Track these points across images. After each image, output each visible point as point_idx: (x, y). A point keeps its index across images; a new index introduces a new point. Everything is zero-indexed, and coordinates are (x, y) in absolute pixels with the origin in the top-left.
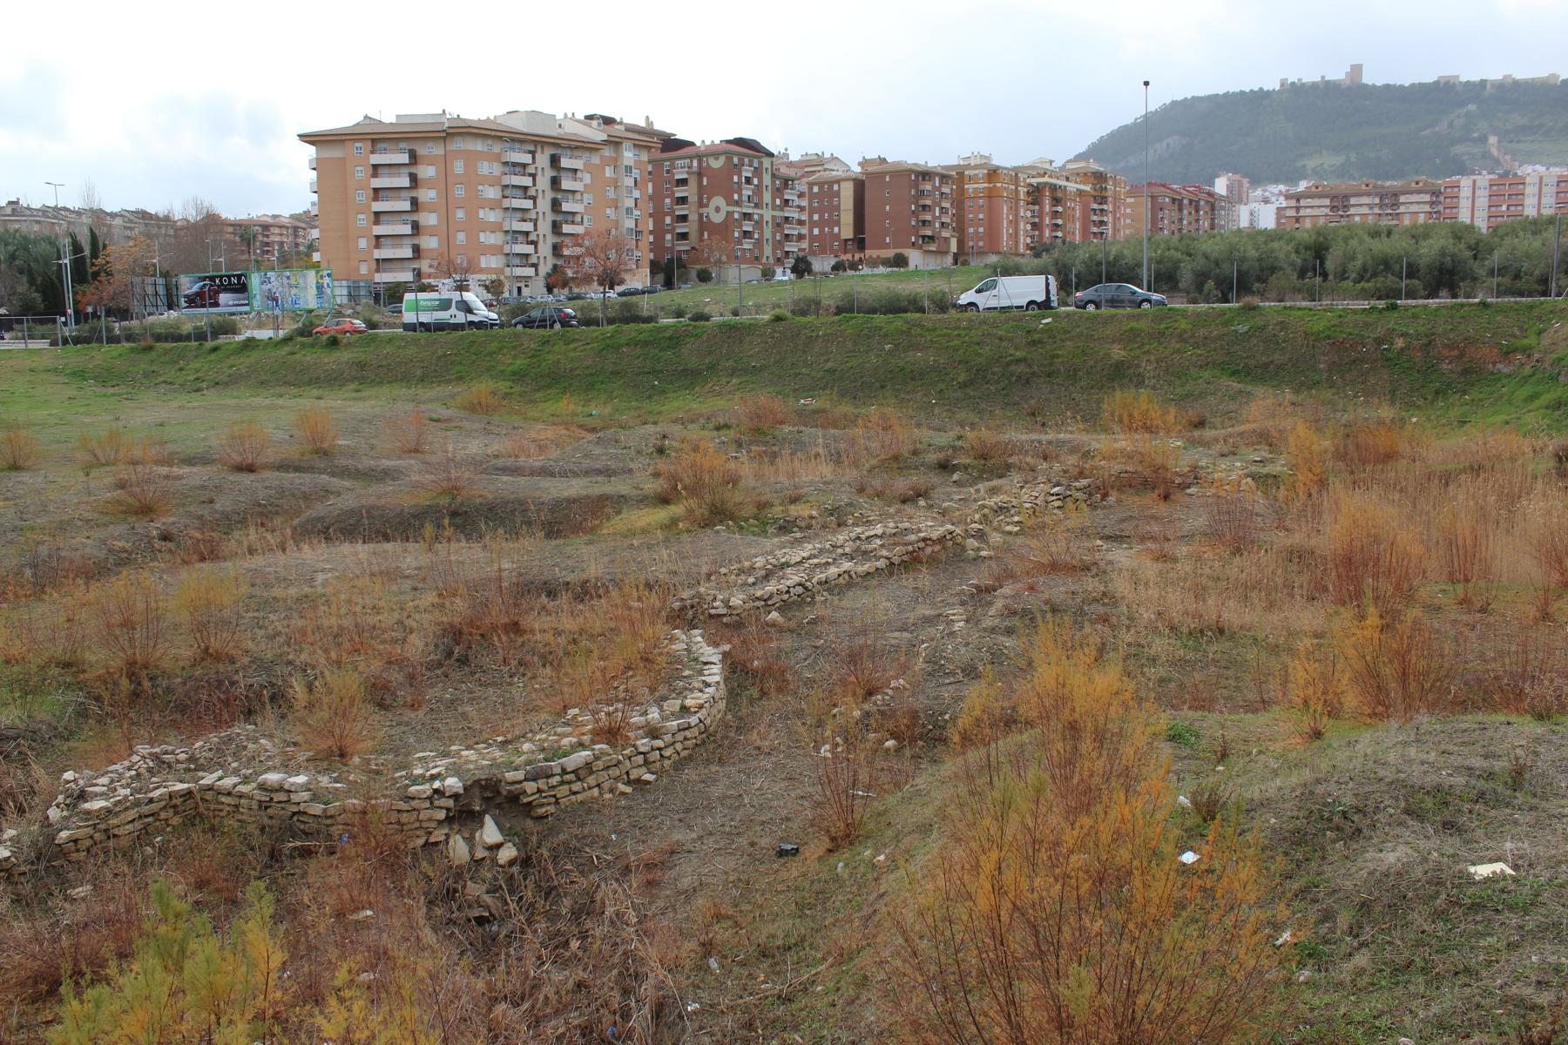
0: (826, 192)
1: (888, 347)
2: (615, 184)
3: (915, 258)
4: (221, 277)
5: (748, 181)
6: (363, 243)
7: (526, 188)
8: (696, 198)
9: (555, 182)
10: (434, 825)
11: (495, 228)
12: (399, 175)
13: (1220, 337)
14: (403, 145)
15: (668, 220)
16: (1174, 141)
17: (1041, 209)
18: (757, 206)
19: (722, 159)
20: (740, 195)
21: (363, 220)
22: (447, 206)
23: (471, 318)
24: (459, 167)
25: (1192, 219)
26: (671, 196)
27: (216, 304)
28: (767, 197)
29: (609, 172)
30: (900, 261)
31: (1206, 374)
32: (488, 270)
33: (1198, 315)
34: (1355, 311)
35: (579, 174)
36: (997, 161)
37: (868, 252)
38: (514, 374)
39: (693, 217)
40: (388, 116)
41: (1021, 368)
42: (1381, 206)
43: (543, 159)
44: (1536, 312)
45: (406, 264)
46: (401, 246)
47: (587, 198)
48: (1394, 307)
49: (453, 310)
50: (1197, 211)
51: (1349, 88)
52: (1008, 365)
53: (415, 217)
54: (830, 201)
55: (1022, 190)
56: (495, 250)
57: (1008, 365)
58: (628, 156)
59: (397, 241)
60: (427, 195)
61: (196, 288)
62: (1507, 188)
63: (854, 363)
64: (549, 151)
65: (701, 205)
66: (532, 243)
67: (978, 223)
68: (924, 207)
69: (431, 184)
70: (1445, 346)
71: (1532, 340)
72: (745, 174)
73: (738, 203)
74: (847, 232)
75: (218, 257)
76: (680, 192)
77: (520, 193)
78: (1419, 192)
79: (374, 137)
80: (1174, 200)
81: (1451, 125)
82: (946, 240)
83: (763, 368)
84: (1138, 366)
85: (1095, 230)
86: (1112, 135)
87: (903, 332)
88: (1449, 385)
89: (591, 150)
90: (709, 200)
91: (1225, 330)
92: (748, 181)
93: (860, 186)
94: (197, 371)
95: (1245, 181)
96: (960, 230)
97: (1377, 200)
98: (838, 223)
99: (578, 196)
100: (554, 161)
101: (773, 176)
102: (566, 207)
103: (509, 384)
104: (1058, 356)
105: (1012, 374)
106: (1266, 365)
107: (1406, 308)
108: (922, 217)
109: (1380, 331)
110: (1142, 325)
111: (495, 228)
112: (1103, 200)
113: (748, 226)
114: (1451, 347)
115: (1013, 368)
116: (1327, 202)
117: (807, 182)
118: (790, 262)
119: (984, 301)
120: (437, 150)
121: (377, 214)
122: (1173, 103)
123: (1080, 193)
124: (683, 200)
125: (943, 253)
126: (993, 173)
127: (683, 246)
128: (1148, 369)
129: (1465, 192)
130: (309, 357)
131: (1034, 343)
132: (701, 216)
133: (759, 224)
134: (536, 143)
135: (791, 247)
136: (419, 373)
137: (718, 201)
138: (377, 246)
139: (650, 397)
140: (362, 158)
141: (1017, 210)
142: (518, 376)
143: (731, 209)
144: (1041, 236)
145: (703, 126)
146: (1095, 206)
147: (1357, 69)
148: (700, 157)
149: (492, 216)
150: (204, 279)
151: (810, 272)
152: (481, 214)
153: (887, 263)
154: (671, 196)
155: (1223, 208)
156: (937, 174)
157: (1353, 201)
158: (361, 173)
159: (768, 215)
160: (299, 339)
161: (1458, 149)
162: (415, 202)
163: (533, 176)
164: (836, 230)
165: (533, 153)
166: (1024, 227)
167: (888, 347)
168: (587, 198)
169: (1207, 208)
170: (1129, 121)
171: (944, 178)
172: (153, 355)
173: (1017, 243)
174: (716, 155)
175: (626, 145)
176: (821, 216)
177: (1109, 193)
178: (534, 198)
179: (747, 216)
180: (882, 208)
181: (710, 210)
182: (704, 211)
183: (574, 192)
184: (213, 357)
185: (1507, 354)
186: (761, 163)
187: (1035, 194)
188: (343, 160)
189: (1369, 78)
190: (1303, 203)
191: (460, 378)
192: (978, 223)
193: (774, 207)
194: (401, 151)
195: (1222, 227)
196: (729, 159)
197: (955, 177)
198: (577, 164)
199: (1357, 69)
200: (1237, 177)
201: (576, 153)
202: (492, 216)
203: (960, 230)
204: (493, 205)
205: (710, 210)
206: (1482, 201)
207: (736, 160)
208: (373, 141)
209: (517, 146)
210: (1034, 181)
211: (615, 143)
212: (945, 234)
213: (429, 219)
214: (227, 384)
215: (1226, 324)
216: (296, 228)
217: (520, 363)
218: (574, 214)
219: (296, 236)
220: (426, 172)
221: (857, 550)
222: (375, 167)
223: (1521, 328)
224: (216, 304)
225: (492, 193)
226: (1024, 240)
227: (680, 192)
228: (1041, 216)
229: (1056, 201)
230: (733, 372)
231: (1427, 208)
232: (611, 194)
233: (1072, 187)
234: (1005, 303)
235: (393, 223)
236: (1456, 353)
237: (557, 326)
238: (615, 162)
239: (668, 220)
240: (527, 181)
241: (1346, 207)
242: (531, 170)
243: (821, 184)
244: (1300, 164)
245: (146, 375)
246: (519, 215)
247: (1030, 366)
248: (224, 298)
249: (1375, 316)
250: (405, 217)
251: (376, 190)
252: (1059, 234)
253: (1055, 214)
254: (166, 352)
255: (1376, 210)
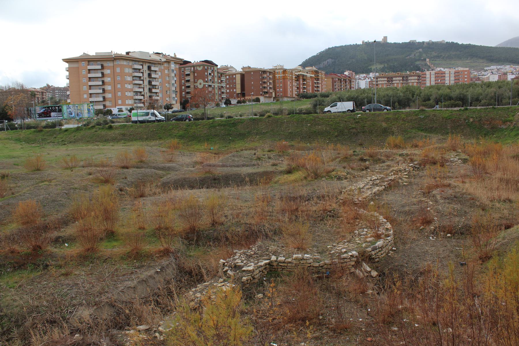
0: (232, 77)
1: (309, 125)
2: (169, 75)
3: (262, 99)
4: (52, 107)
5: (210, 74)
6: (85, 96)
7: (140, 77)
8: (193, 80)
9: (150, 75)
10: (351, 266)
11: (130, 90)
12: (97, 73)
13: (416, 119)
14: (99, 63)
15: (183, 87)
16: (330, 61)
17: (299, 83)
18: (213, 82)
19: (202, 67)
20: (208, 79)
21: (85, 88)
22: (114, 83)
23: (157, 118)
24: (118, 70)
25: (344, 85)
26: (184, 79)
27: (50, 116)
28: (216, 80)
29: (166, 72)
30: (258, 100)
31: (414, 131)
32: (129, 105)
33: (407, 113)
34: (455, 111)
35: (157, 72)
36: (286, 67)
37: (246, 98)
38: (180, 136)
39: (192, 86)
40: (92, 53)
41: (354, 130)
42: (403, 80)
43: (146, 67)
44: (510, 110)
45: (101, 103)
46: (98, 97)
47: (160, 80)
48: (467, 109)
49: (150, 116)
50: (346, 83)
51: (383, 44)
52: (350, 129)
53: (103, 87)
54: (233, 81)
55: (294, 77)
56: (131, 98)
57: (350, 129)
58: (173, 66)
59: (97, 95)
60: (107, 80)
61: (42, 111)
62: (440, 75)
63: (298, 130)
64: (147, 65)
65: (195, 82)
66: (143, 95)
67: (280, 87)
68: (264, 82)
69: (108, 75)
70: (485, 120)
71: (511, 118)
72: (209, 72)
73: (207, 82)
74: (238, 90)
75: (49, 102)
76: (187, 78)
77: (138, 79)
78: (414, 76)
79: (88, 60)
80: (339, 79)
81: (415, 55)
82: (271, 93)
83: (267, 132)
84: (392, 129)
85: (316, 89)
86: (310, 59)
87: (313, 120)
88: (488, 132)
89: (160, 64)
90: (197, 80)
91: (417, 117)
92: (210, 74)
93: (243, 76)
94: (62, 138)
95: (354, 73)
96: (275, 89)
97: (401, 78)
98: (235, 88)
99: (157, 80)
100: (149, 68)
101: (218, 72)
102: (153, 83)
103: (179, 140)
104: (365, 126)
105: (351, 132)
106: (431, 128)
107: (471, 109)
108: (264, 86)
109: (465, 117)
110: (390, 116)
111: (130, 90)
112: (318, 79)
113: (210, 89)
114: (487, 121)
115: (351, 130)
116: (386, 79)
117: (225, 74)
118: (224, 101)
119: (333, 110)
120: (110, 64)
121: (90, 86)
122: (329, 48)
123: (311, 77)
124: (188, 81)
125: (270, 97)
126: (285, 71)
127: (189, 96)
128: (395, 129)
129: (428, 76)
130: (103, 132)
131: (357, 122)
132: (195, 86)
133: (214, 88)
134: (143, 62)
135: (224, 96)
136: (145, 137)
137: (201, 81)
138: (91, 97)
139: (229, 143)
140: (85, 66)
141: (292, 83)
142: (181, 137)
143: (205, 83)
144: (300, 91)
145: (194, 56)
146: (316, 81)
147: (385, 38)
148: (194, 67)
149: (129, 87)
150: (45, 108)
151: (230, 104)
152: (126, 86)
153: (254, 101)
154: (184, 79)
155: (353, 82)
156: (268, 72)
157: (394, 79)
158: (84, 72)
159: (216, 85)
160: (97, 126)
161: (417, 63)
162: (103, 82)
163: (143, 73)
164: (235, 90)
165: (142, 65)
166: (295, 88)
167: (309, 125)
168: (160, 80)
169: (349, 82)
170: (315, 54)
171: (270, 73)
172: (43, 133)
173: (293, 93)
174: (200, 66)
175: (172, 63)
176: (230, 86)
177: (320, 77)
178: (143, 80)
179: (210, 86)
180: (250, 83)
181: (198, 84)
182: (196, 84)
183: (155, 78)
184: (66, 133)
185: (505, 122)
186: (214, 68)
187: (298, 77)
188: (78, 67)
189: (389, 41)
190: (379, 79)
191: (160, 138)
192: (280, 87)
193: (218, 83)
194: (98, 65)
195: (353, 88)
196: (204, 67)
197: (272, 72)
198: (156, 69)
199: (385, 38)
200: (351, 72)
201: (156, 65)
202: (129, 87)
203: (275, 89)
204: (130, 83)
205: (198, 84)
206: (433, 79)
207: (206, 67)
208: (88, 61)
209: (137, 63)
210: (297, 74)
211: (168, 62)
212: (271, 91)
213: (108, 88)
214: (74, 142)
215: (417, 115)
216: (42, 92)
217: (181, 133)
218: (155, 85)
219: (43, 95)
220: (107, 72)
221: (373, 184)
222: (89, 70)
223: (507, 115)
224: (50, 116)
225: (129, 79)
226: (295, 93)
227: (187, 78)
228: (299, 85)
229: (304, 80)
230: (257, 134)
231: (417, 81)
232: (167, 79)
233: (309, 75)
234: (339, 110)
235: (96, 89)
236: (489, 122)
237: (187, 121)
238: (168, 68)
239: (183, 87)
240: (141, 75)
241: (392, 81)
242: (142, 71)
243: (229, 75)
244: (370, 68)
245: (43, 140)
246: (138, 86)
247: (357, 130)
248: (53, 114)
249: (461, 113)
250: (100, 87)
251: (90, 78)
252: (305, 91)
253: (304, 84)
254: (48, 132)
255: (401, 82)
